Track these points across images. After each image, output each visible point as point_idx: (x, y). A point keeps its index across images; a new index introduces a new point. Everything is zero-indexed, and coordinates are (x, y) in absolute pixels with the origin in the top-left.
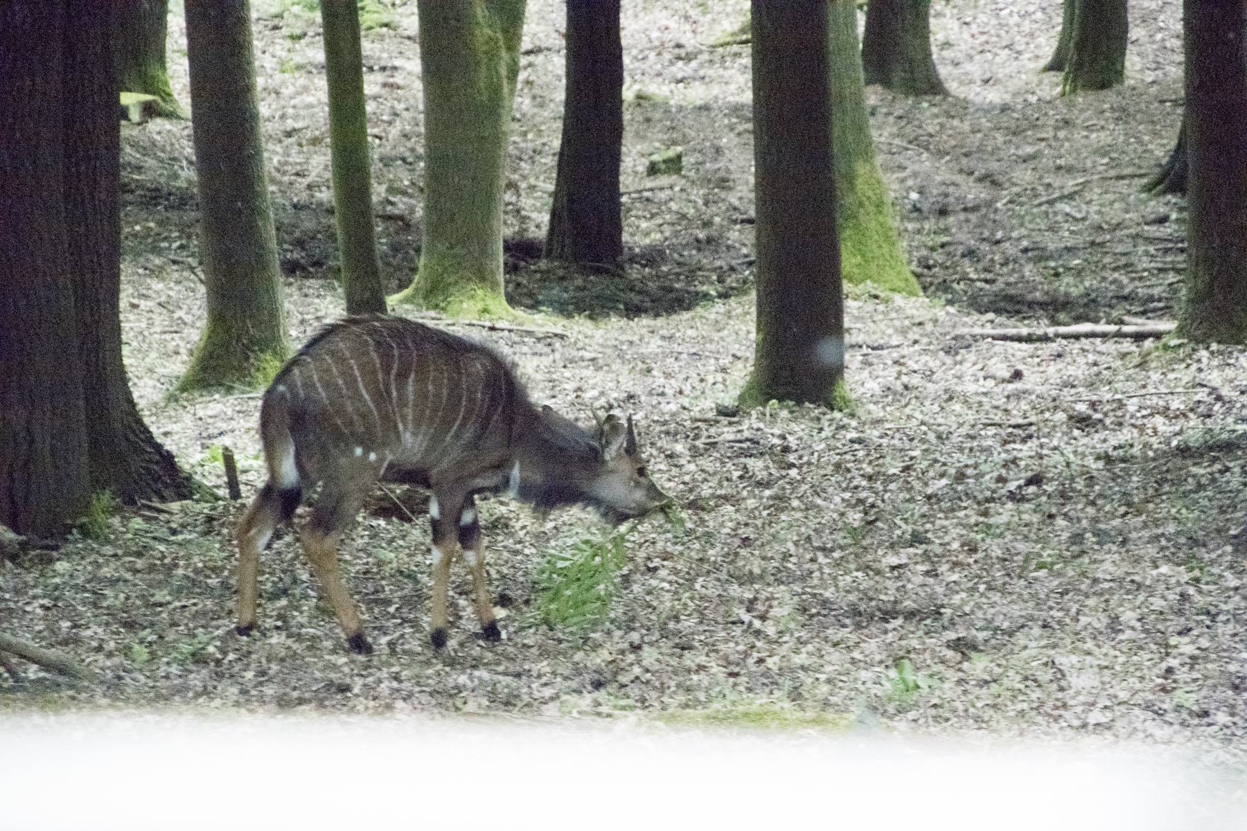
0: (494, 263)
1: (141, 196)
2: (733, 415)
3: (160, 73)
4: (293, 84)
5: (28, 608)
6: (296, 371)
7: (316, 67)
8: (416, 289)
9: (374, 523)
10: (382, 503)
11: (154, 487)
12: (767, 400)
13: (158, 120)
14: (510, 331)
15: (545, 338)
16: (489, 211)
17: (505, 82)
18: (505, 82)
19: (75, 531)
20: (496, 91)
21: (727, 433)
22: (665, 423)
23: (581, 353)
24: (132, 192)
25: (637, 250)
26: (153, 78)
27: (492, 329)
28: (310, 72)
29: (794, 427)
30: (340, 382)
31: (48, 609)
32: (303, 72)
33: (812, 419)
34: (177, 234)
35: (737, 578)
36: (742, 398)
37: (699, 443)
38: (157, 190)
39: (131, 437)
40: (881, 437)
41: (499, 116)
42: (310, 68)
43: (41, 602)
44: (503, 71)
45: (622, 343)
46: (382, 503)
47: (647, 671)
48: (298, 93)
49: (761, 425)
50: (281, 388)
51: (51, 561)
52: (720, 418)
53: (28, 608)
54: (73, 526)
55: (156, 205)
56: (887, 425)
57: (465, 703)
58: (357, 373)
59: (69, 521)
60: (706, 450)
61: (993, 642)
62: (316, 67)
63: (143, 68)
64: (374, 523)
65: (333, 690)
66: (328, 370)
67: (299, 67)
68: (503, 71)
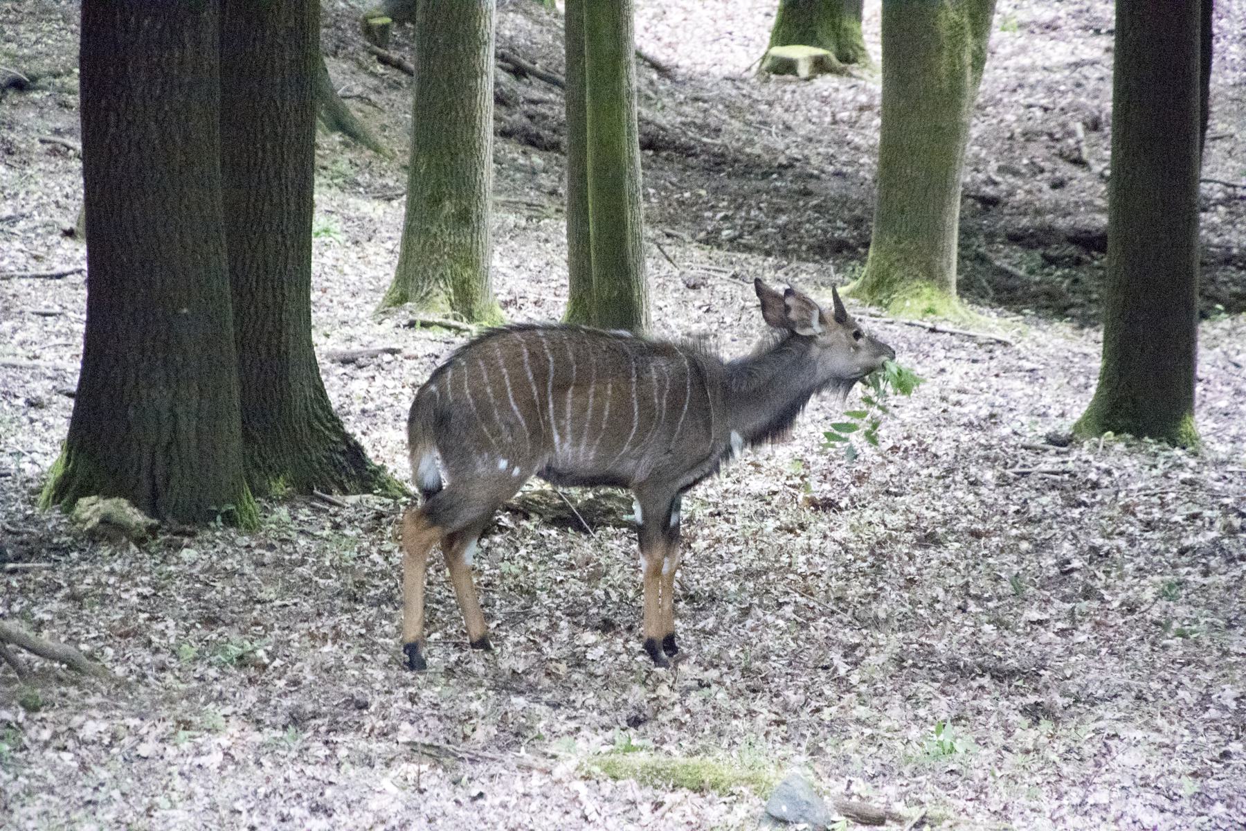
0: (945, 260)
1: (705, 161)
2: (1064, 444)
3: (854, 26)
4: (1012, 44)
5: (124, 596)
6: (450, 374)
7: (1040, 26)
8: (864, 283)
9: (545, 532)
10: (560, 513)
11: (337, 477)
12: (1105, 431)
13: (829, 77)
14: (952, 334)
15: (987, 344)
16: (943, 206)
17: (969, 70)
18: (969, 70)
19: (219, 518)
20: (956, 77)
21: (1050, 462)
22: (990, 447)
23: (1021, 363)
24: (695, 155)
25: (1235, 251)
26: (846, 30)
27: (933, 330)
28: (1032, 32)
29: (1127, 462)
30: (489, 390)
31: (145, 597)
32: (1025, 31)
33: (1149, 455)
34: (725, 203)
35: (862, 621)
36: (1077, 427)
37: (1009, 472)
38: (723, 155)
39: (316, 424)
40: (1218, 480)
41: (960, 106)
42: (1033, 27)
43: (140, 590)
44: (968, 59)
45: (1075, 355)
46: (560, 513)
47: (688, 711)
48: (1013, 54)
49: (1091, 458)
50: (433, 388)
51: (179, 547)
52: (1047, 446)
53: (124, 596)
54: (217, 512)
55: (719, 172)
56: (1230, 468)
57: (474, 730)
58: (507, 382)
59: (214, 508)
60: (1015, 479)
61: (1073, 709)
62: (1040, 26)
63: (837, 20)
64: (545, 532)
65: (352, 706)
66: (479, 377)
67: (1021, 26)
68: (968, 59)
